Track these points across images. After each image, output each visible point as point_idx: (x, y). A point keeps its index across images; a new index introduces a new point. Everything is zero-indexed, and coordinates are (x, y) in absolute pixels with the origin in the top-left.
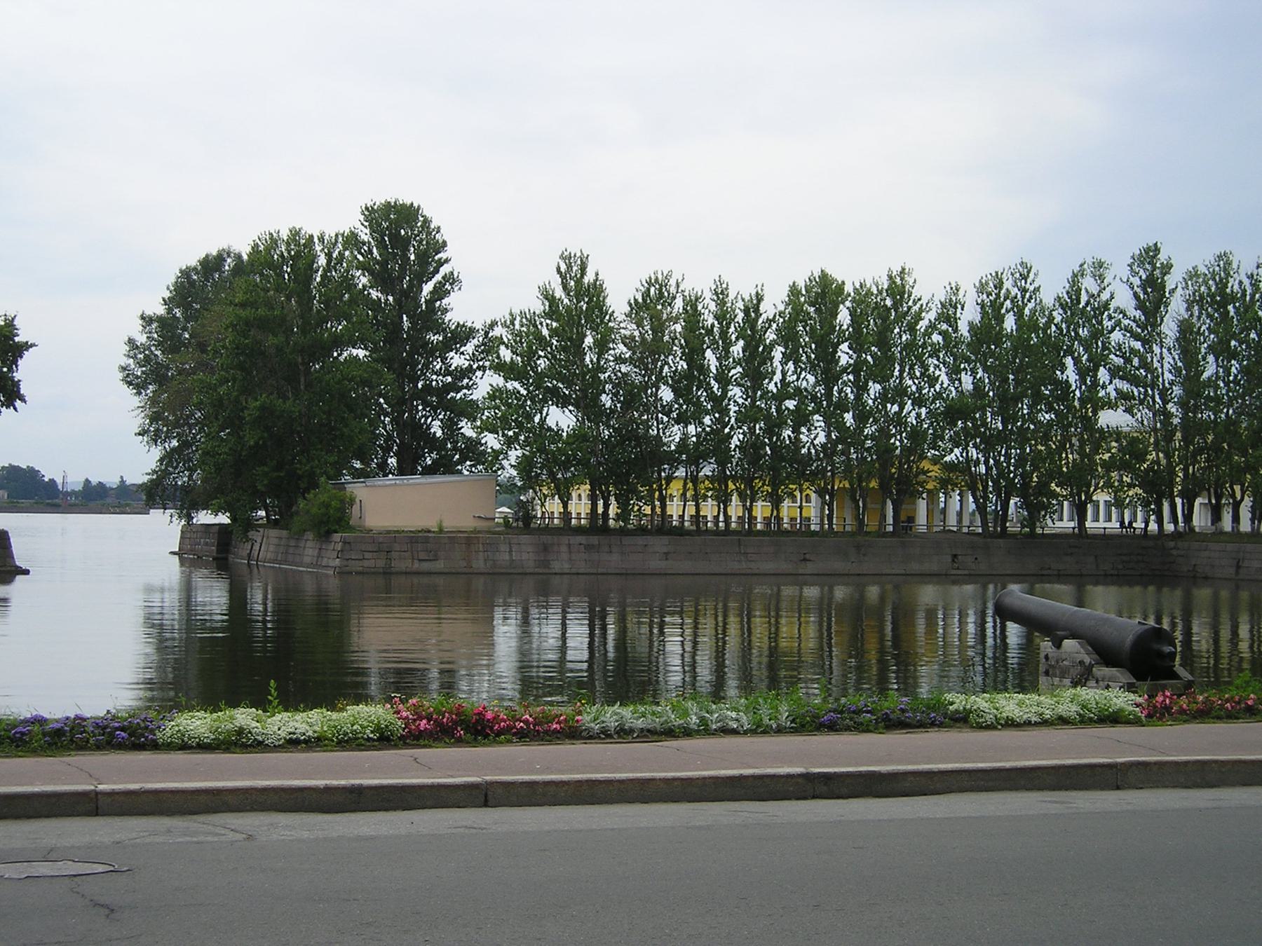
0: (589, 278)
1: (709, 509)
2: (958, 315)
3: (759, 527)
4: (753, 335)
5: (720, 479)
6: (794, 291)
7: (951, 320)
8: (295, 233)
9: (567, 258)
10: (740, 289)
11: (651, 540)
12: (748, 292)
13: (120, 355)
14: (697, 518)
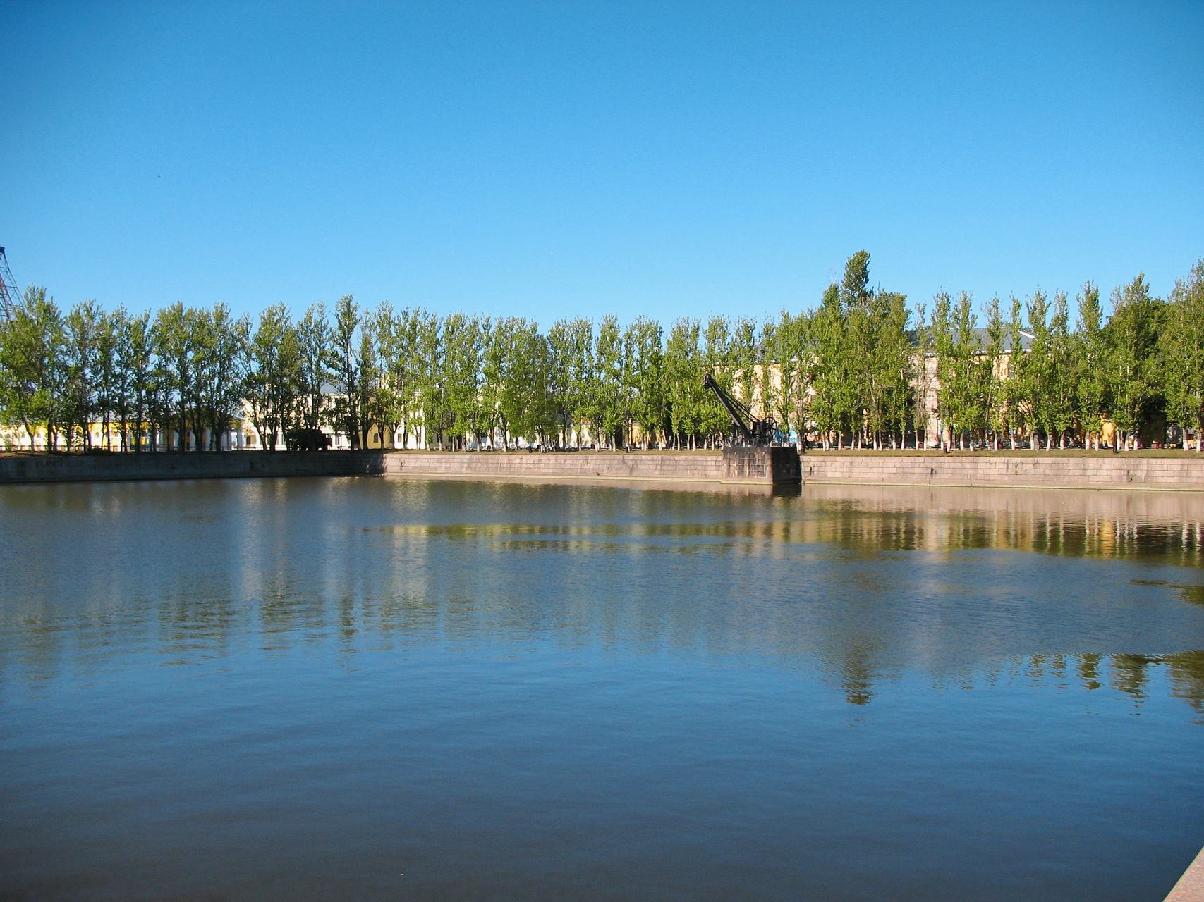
9: (33, 291)
10: (134, 314)
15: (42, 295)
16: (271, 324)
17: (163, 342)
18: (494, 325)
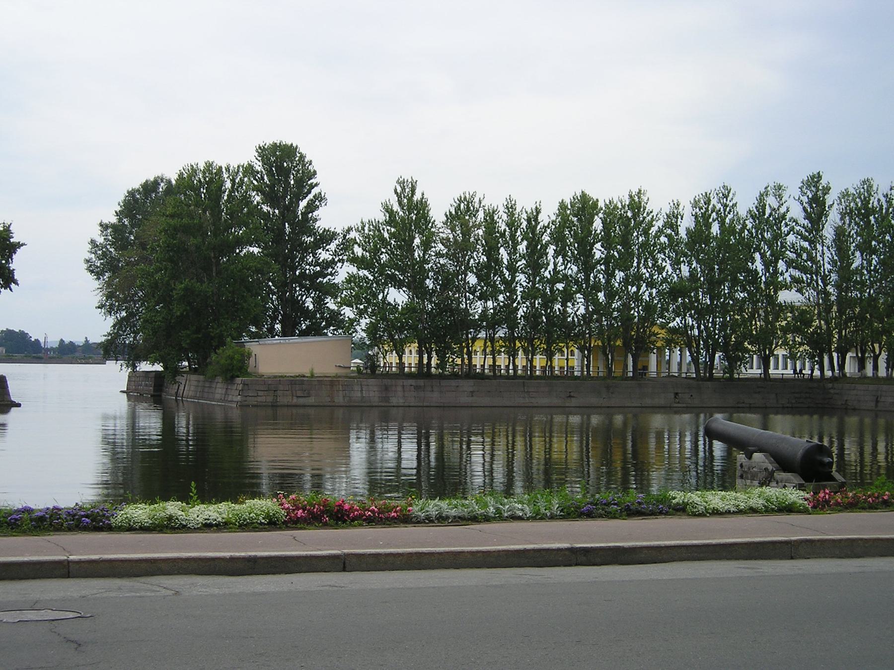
0: (417, 197)
1: (502, 360)
2: (679, 223)
3: (538, 373)
4: (533, 237)
5: (510, 339)
6: (562, 206)
7: (674, 227)
8: (209, 165)
9: (401, 183)
10: (524, 205)
11: (461, 382)
12: (530, 207)
13: (85, 252)
14: (494, 367)
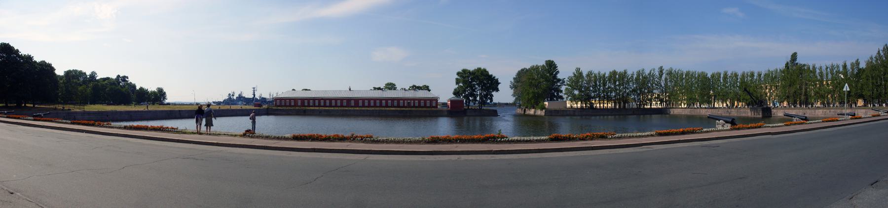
0: (580, 71)
4: (604, 80)
6: (610, 72)
8: (537, 65)
9: (577, 68)
10: (602, 73)
12: (603, 73)
13: (509, 84)
14: (600, 106)
15: (579, 70)
16: (639, 74)
17: (609, 80)
18: (824, 68)
